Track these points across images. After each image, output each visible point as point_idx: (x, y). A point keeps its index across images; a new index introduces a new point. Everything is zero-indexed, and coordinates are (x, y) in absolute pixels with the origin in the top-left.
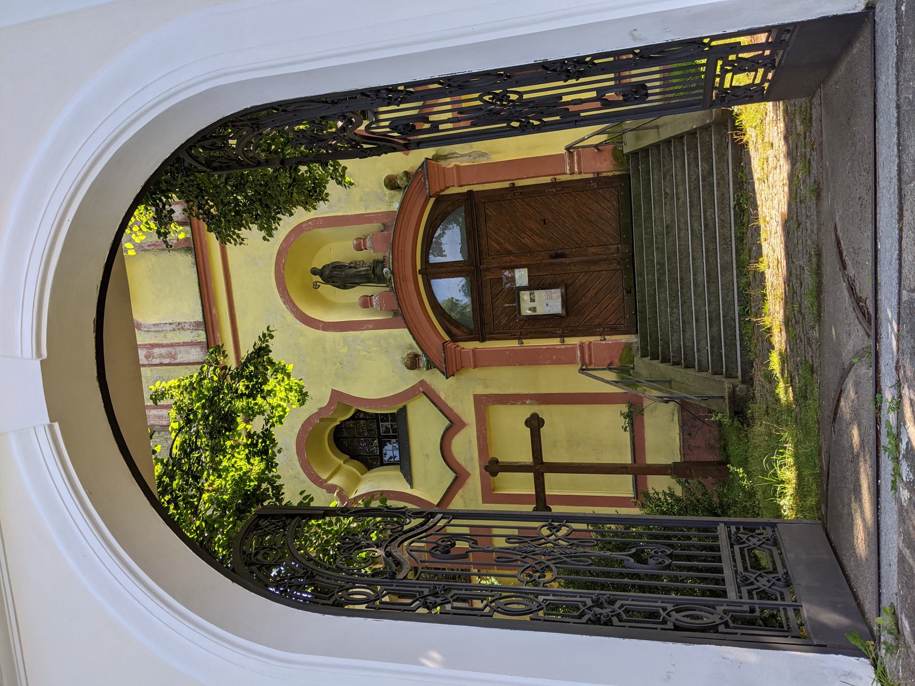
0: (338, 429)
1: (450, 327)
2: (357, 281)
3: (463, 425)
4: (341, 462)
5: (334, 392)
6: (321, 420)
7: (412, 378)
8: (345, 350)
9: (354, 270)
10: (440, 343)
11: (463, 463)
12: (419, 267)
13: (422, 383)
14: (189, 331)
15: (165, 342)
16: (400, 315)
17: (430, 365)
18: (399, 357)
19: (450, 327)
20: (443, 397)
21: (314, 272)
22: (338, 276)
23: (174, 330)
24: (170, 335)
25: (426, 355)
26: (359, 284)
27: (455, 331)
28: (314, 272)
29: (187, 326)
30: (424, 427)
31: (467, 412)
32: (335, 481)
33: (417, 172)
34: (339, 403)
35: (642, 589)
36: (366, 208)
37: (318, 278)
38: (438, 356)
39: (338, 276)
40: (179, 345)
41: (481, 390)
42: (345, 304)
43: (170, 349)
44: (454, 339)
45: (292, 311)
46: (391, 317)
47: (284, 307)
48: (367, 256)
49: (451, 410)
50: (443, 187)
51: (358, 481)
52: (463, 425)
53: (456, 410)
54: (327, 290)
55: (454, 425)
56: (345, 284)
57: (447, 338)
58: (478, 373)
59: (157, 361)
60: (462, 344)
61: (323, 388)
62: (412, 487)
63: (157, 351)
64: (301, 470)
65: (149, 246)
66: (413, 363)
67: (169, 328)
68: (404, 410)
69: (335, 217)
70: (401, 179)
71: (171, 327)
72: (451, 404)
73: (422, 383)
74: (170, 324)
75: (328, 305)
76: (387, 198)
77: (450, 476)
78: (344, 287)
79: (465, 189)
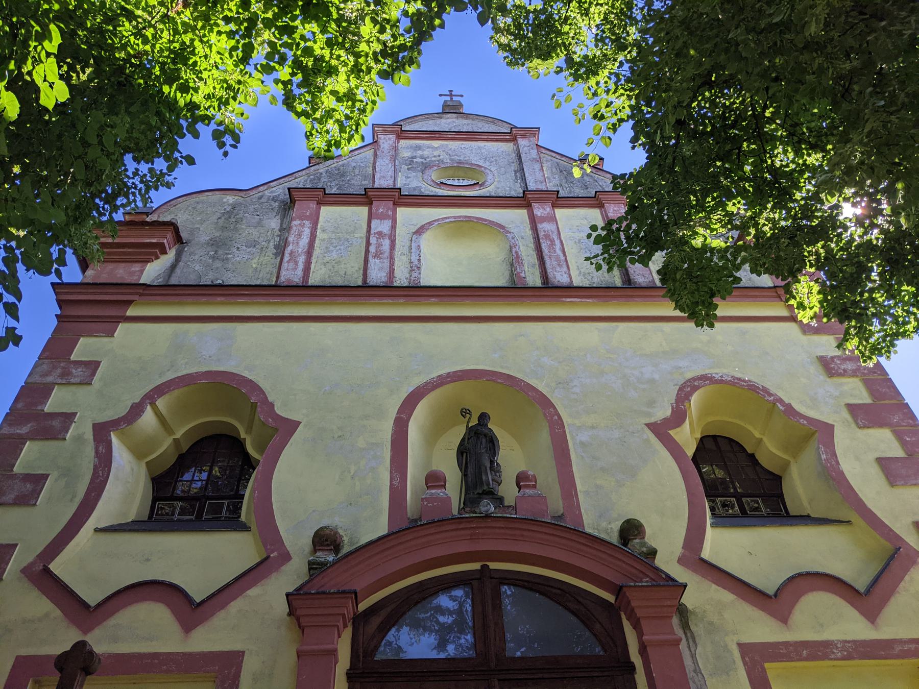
0: (237, 444)
1: (384, 613)
2: (470, 471)
3: (188, 626)
4: (178, 435)
5: (294, 425)
6: (254, 406)
7: (297, 541)
8: (361, 443)
9: (488, 465)
10: (359, 585)
11: (112, 621)
12: (493, 565)
13: (286, 557)
14: (408, 276)
15: (397, 254)
16: (407, 529)
17: (315, 568)
18: (338, 521)
19: (384, 613)
20: (252, 592)
21: (484, 417)
22: (477, 448)
23: (411, 262)
24: (405, 259)
25: (335, 563)
26: (465, 475)
27: (376, 621)
28: (484, 417)
29: (414, 275)
30: (198, 558)
31: (209, 638)
32: (148, 418)
33: (657, 570)
34: (277, 430)
35: (506, 579)
36: (587, 493)
37: (474, 422)
38: (332, 582)
39: (477, 448)
40: (392, 264)
41: (250, 666)
42: (434, 453)
43: (387, 254)
44: (359, 620)
45: (427, 384)
46: (409, 515)
47: (435, 375)
48: (508, 490)
49: (224, 605)
50: (639, 613)
51: (138, 452)
52: (188, 626)
53: (222, 614)
54: (458, 433)
55: (190, 610)
56: (463, 452)
57: (362, 607)
58: (288, 659)
59: (373, 240)
60: (347, 634)
61: (305, 411)
62: (97, 530)
63: (386, 243)
64: (180, 374)
65: (516, 252)
66: (325, 539)
67: (414, 258)
68: (244, 528)
69: (568, 450)
70: (644, 544)
71: (414, 258)
72: (236, 606)
73: (286, 557)
74: (419, 260)
75: (434, 433)
76: (604, 524)
77: (92, 597)
78: (462, 451)
79: (635, 658)
